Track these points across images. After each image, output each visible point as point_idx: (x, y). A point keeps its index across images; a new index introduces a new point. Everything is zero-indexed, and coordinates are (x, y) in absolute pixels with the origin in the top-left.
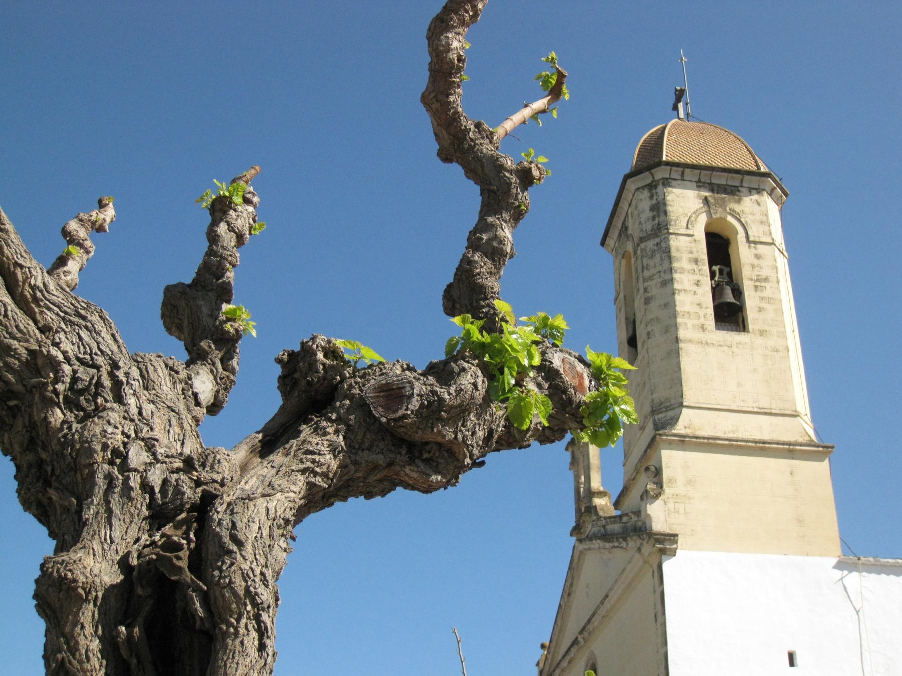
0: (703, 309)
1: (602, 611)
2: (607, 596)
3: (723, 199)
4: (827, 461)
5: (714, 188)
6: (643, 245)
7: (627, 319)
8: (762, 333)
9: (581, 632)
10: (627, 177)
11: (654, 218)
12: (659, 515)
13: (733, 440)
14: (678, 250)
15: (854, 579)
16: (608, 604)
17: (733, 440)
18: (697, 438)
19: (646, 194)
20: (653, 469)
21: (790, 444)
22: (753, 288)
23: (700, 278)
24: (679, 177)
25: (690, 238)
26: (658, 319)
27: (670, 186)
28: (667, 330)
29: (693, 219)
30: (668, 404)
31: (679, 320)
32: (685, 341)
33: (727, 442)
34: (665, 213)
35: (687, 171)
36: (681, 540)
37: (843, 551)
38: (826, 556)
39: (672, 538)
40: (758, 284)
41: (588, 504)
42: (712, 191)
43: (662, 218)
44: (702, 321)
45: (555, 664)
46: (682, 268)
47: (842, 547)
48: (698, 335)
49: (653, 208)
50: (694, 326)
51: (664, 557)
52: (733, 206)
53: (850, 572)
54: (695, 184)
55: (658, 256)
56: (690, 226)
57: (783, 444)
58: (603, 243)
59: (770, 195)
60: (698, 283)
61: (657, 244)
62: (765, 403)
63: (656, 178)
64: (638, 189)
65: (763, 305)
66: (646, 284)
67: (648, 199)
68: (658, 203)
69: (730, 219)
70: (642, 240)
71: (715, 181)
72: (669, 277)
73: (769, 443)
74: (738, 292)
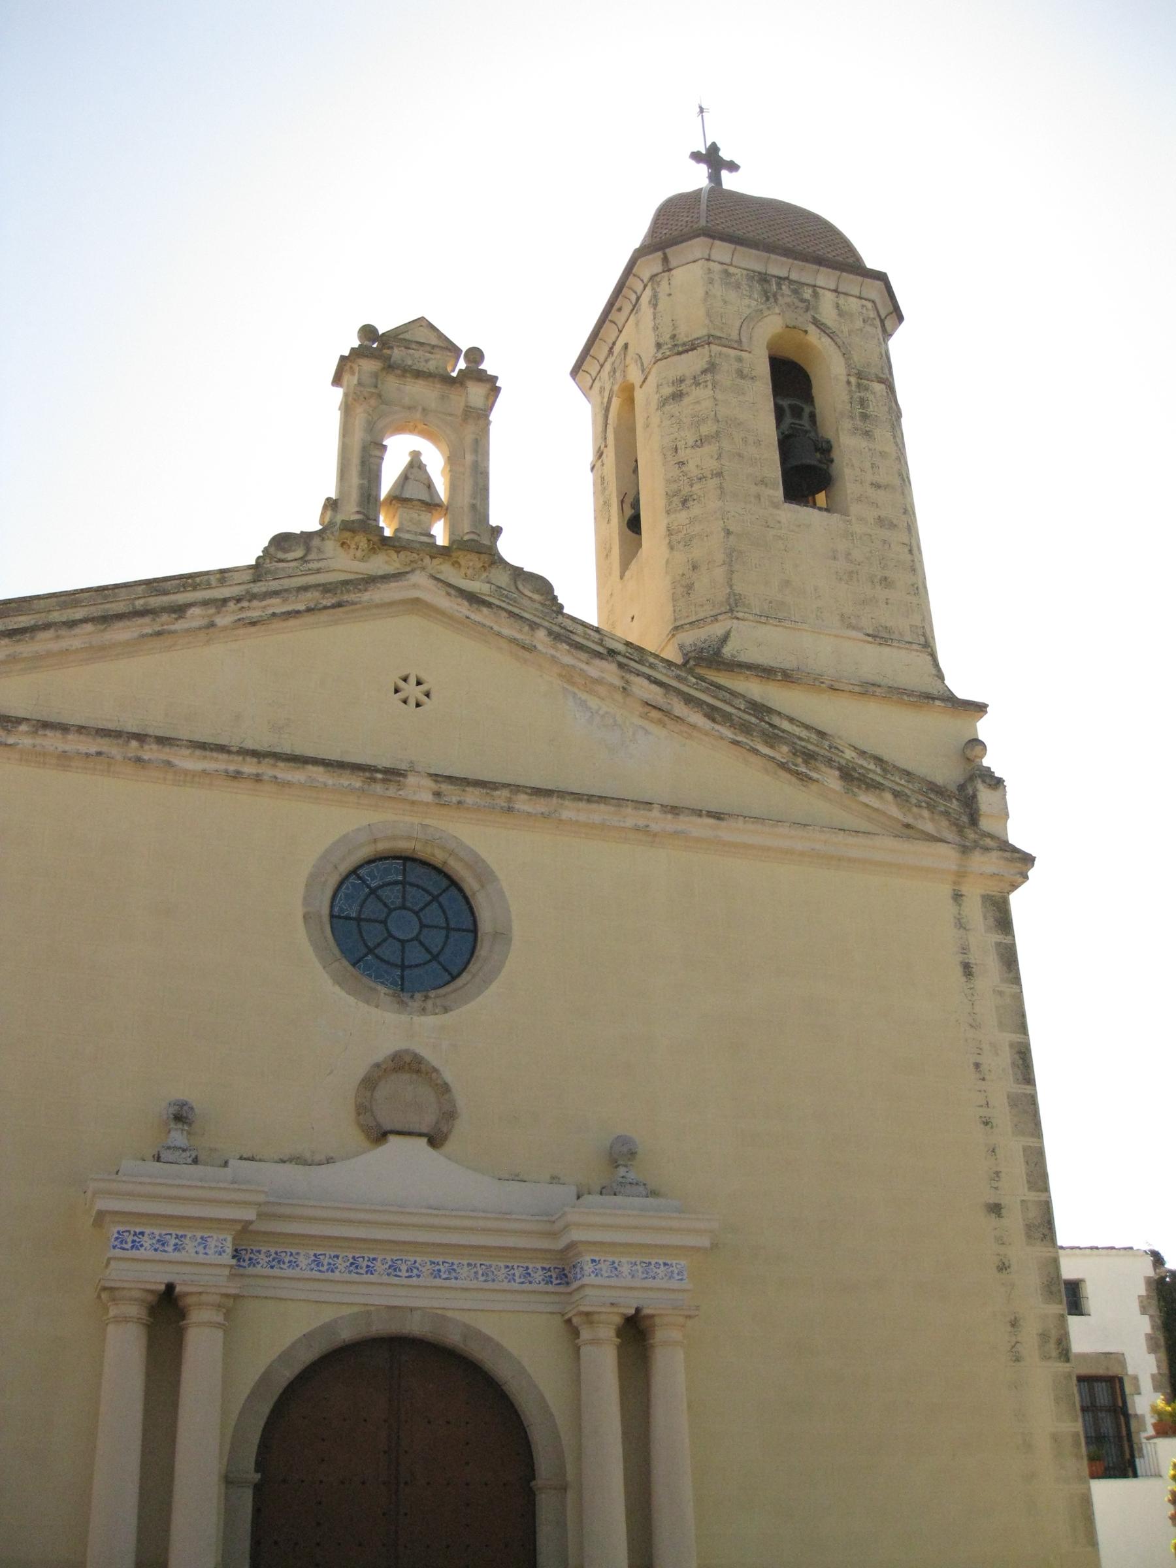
2: (718, 816)
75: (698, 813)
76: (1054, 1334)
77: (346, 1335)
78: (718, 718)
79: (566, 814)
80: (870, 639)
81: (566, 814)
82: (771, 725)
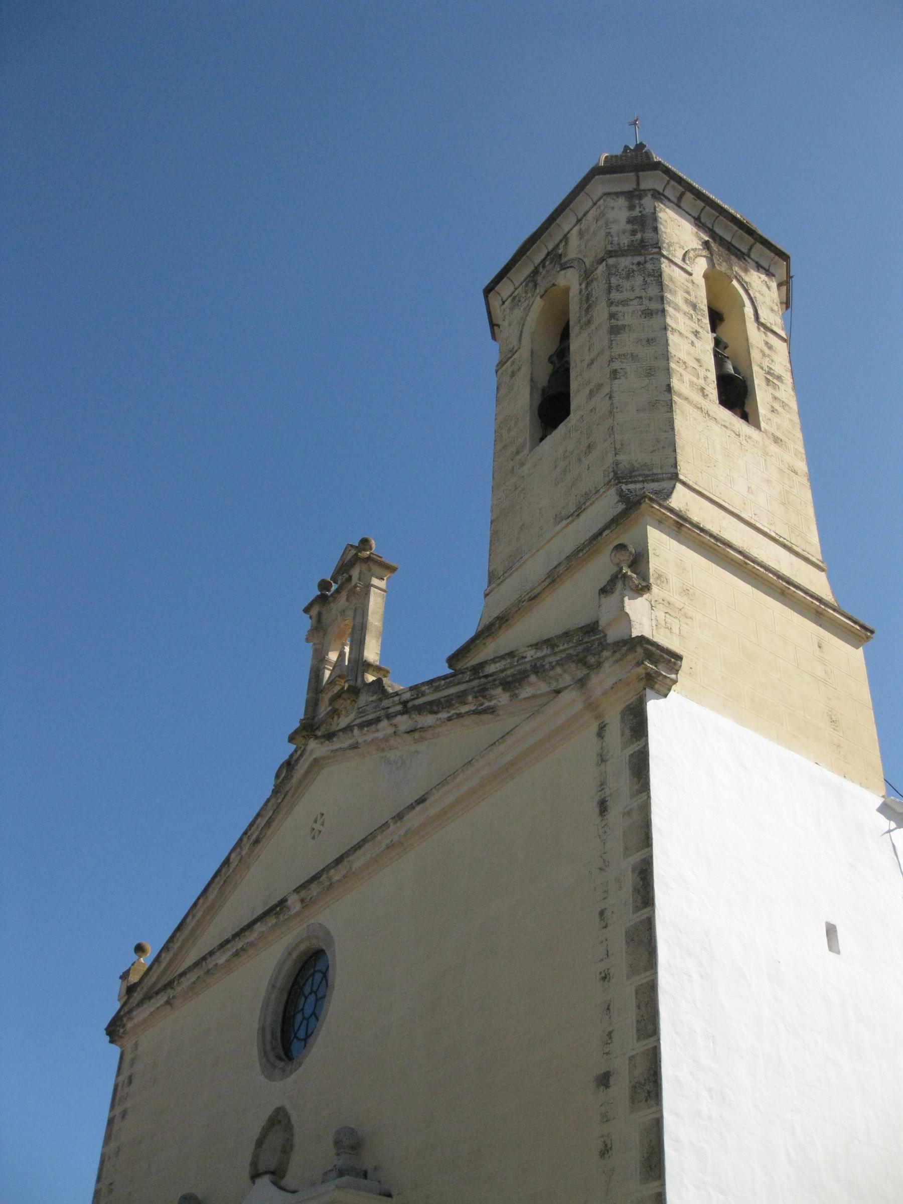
1: (383, 840)
2: (422, 800)
4: (861, 648)
6: (611, 261)
9: (297, 890)
10: (596, 171)
11: (634, 233)
14: (671, 279)
16: (414, 819)
19: (622, 202)
26: (634, 357)
27: (662, 203)
28: (650, 372)
34: (656, 230)
35: (688, 195)
38: (868, 788)
45: (163, 982)
48: (697, 397)
57: (812, 596)
61: (639, 264)
63: (642, 187)
64: (608, 194)
66: (614, 309)
70: (611, 254)
71: (718, 230)
72: (660, 307)
75: (411, 807)
78: (435, 708)
79: (357, 865)
80: (570, 519)
81: (357, 865)
82: (486, 676)
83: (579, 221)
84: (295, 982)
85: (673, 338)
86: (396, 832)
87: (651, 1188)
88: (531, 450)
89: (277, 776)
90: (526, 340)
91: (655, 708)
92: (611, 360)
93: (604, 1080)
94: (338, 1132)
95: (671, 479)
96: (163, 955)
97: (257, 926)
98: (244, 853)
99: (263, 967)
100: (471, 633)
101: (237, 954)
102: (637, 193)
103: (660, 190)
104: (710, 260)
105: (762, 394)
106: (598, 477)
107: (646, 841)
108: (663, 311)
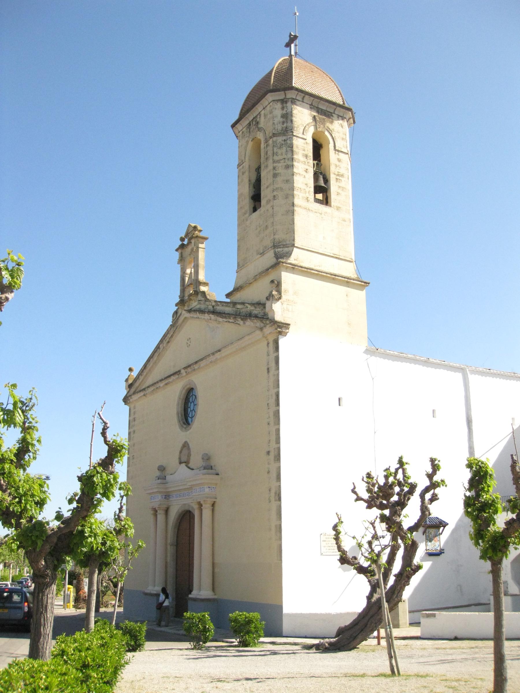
0: (308, 188)
1: (210, 359)
2: (219, 351)
3: (324, 119)
5: (319, 111)
6: (275, 139)
7: (250, 181)
8: (338, 208)
9: (185, 368)
11: (283, 123)
12: (279, 311)
13: (320, 272)
14: (297, 147)
15: (376, 361)
16: (218, 355)
17: (320, 272)
18: (302, 267)
19: (279, 105)
20: (276, 282)
21: (348, 278)
22: (335, 179)
23: (308, 167)
24: (301, 99)
25: (304, 141)
26: (282, 189)
29: (307, 128)
30: (284, 243)
31: (295, 192)
32: (297, 206)
33: (317, 272)
35: (307, 96)
36: (291, 328)
37: (368, 344)
39: (287, 326)
40: (338, 177)
41: (195, 289)
42: (318, 112)
43: (289, 124)
44: (307, 195)
46: (299, 160)
47: (368, 342)
49: (283, 116)
50: (303, 197)
51: (280, 336)
52: (328, 124)
53: (371, 356)
54: (308, 106)
55: (284, 148)
56: (305, 133)
57: (344, 278)
58: (233, 126)
59: (347, 122)
60: (306, 171)
61: (285, 140)
62: (336, 251)
63: (288, 97)
65: (340, 191)
66: (275, 165)
67: (280, 110)
68: (287, 114)
69: (327, 133)
70: (274, 135)
71: (321, 106)
73: (338, 276)
74: (326, 181)
76: (278, 492)
77: (180, 511)
83: (264, 108)
84: (187, 397)
85: (296, 178)
86: (212, 358)
87: (278, 484)
88: (250, 214)
89: (173, 317)
90: (247, 159)
91: (282, 341)
92: (273, 191)
93: (268, 453)
94: (203, 455)
95: (292, 246)
96: (140, 377)
97: (172, 377)
98: (164, 345)
99: (175, 391)
100: (232, 289)
101: (166, 384)
102: (285, 100)
103: (294, 98)
104: (316, 127)
105: (334, 187)
106: (268, 242)
107: (278, 386)
108: (293, 165)
